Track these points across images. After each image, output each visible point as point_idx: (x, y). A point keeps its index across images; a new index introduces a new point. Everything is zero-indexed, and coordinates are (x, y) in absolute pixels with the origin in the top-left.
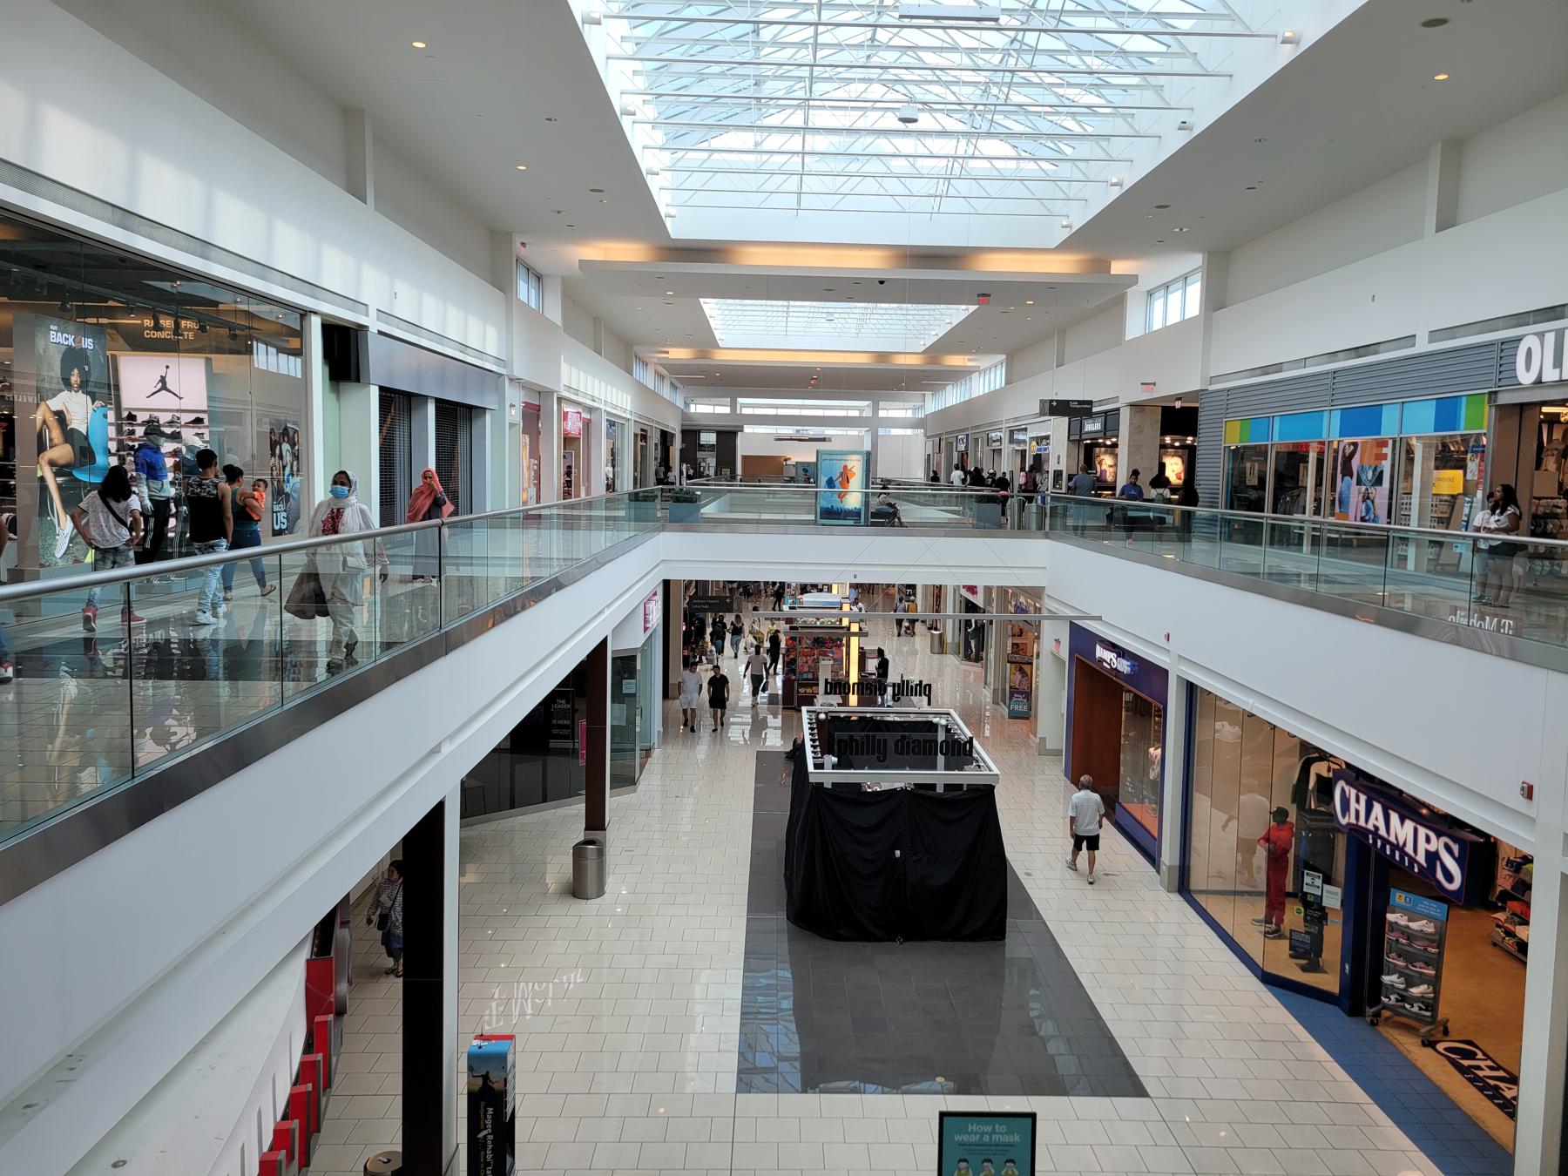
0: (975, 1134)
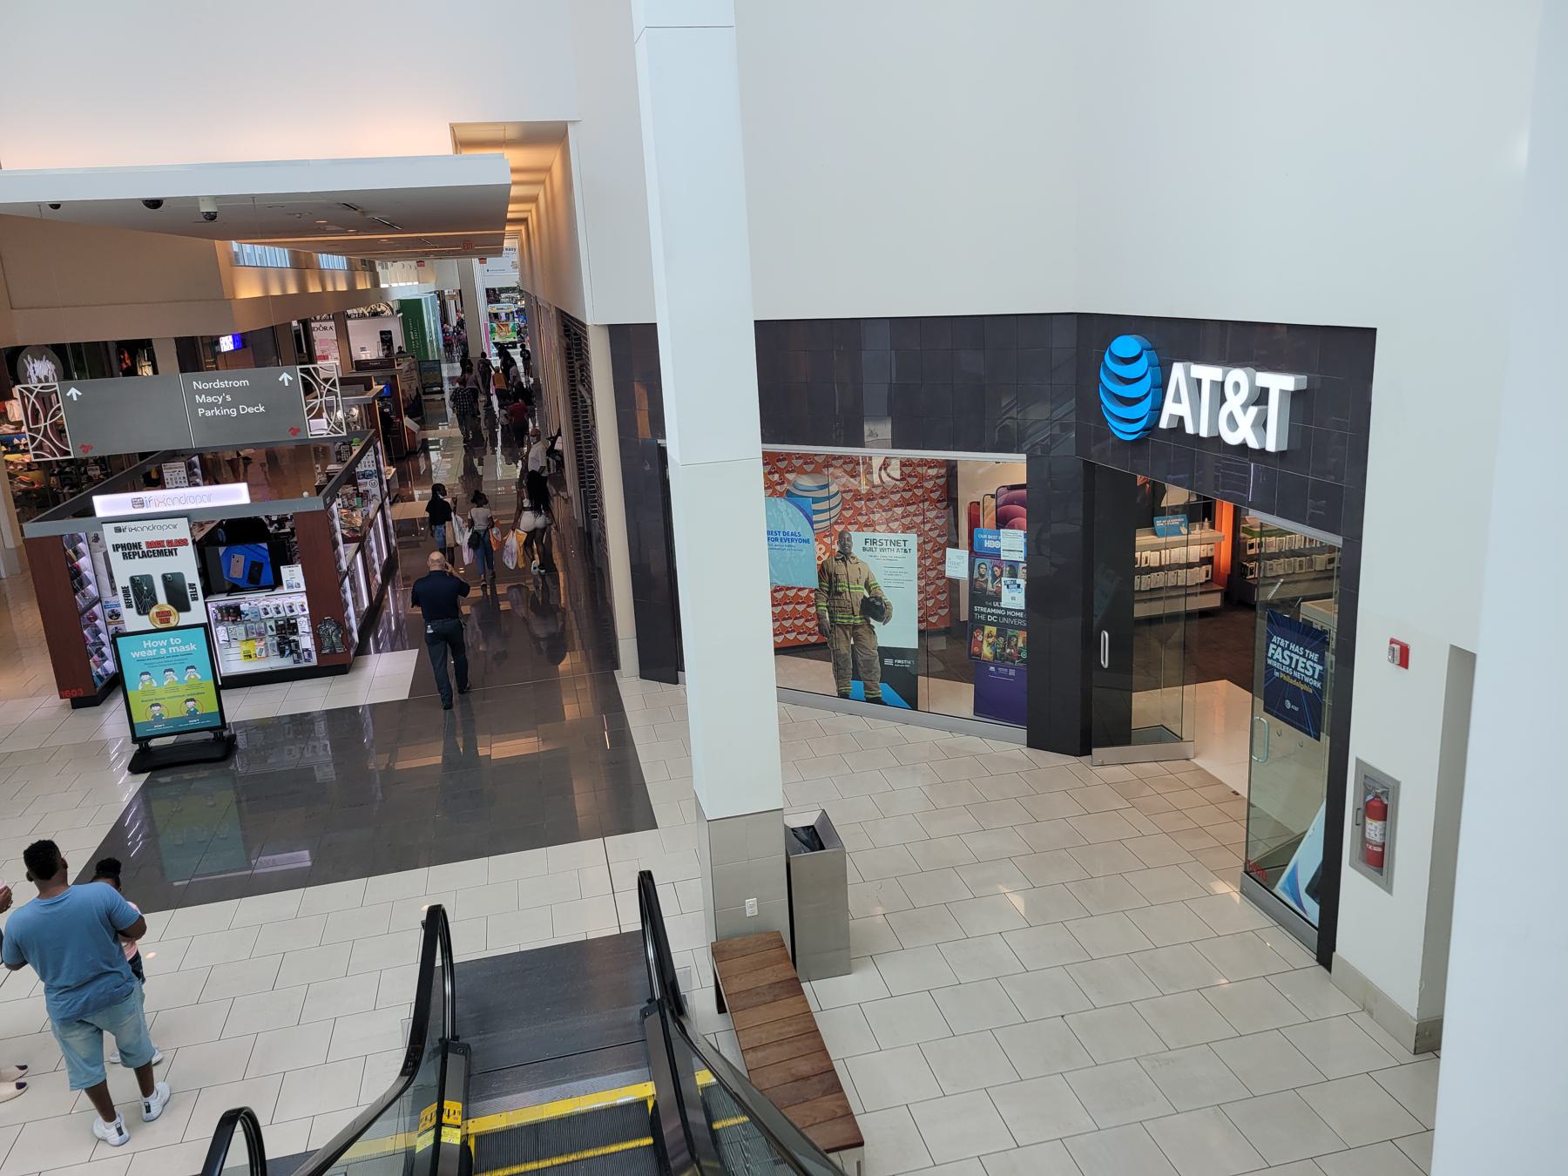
0: (152, 648)
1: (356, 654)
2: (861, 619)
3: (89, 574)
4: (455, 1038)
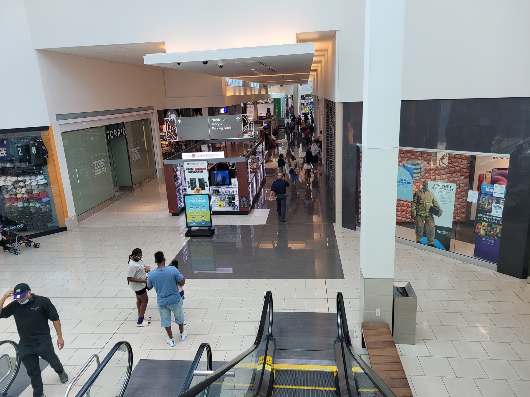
1: (251, 209)
2: (429, 214)
3: (179, 176)
4: (272, 336)
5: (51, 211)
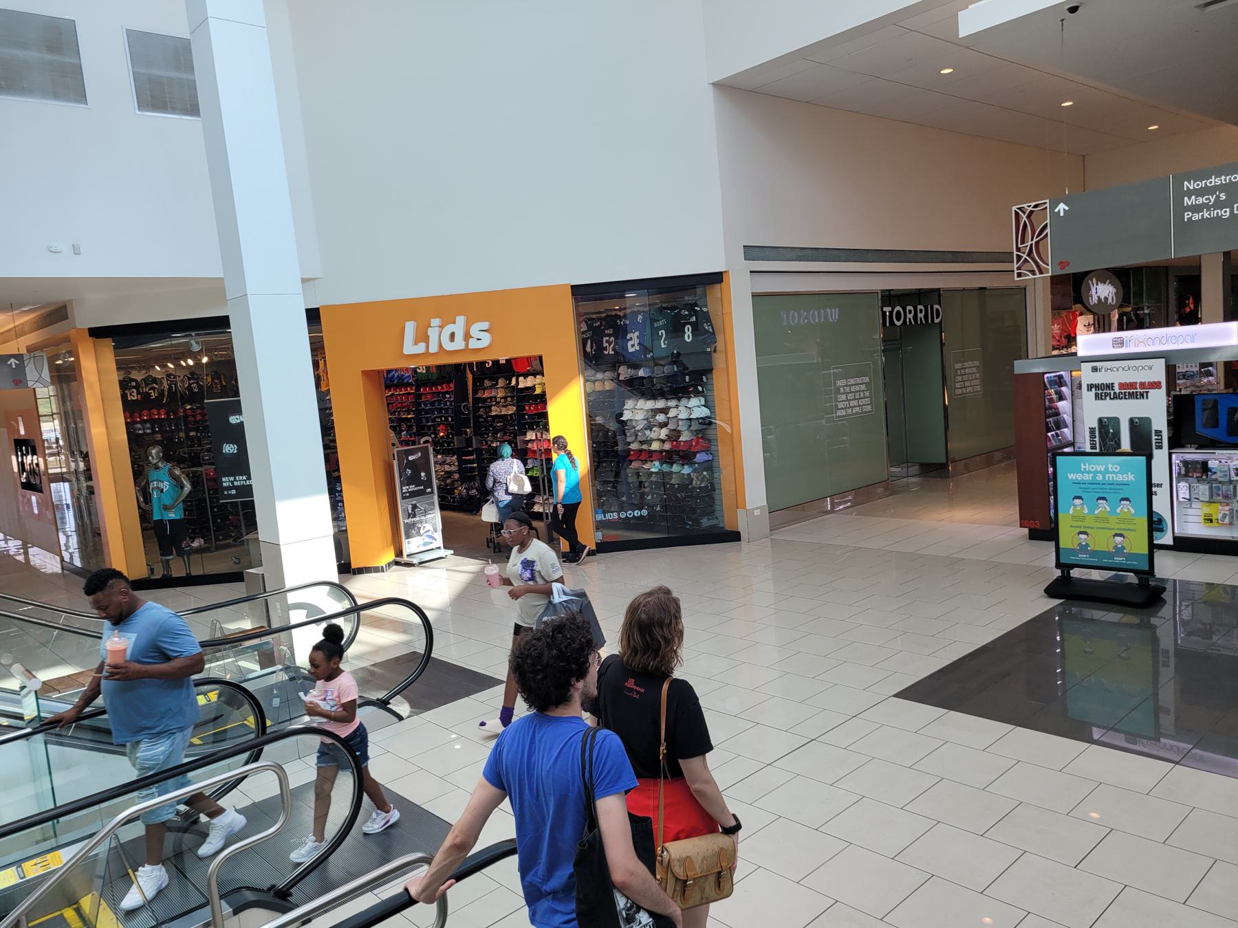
0: (1089, 472)
5: (713, 489)
